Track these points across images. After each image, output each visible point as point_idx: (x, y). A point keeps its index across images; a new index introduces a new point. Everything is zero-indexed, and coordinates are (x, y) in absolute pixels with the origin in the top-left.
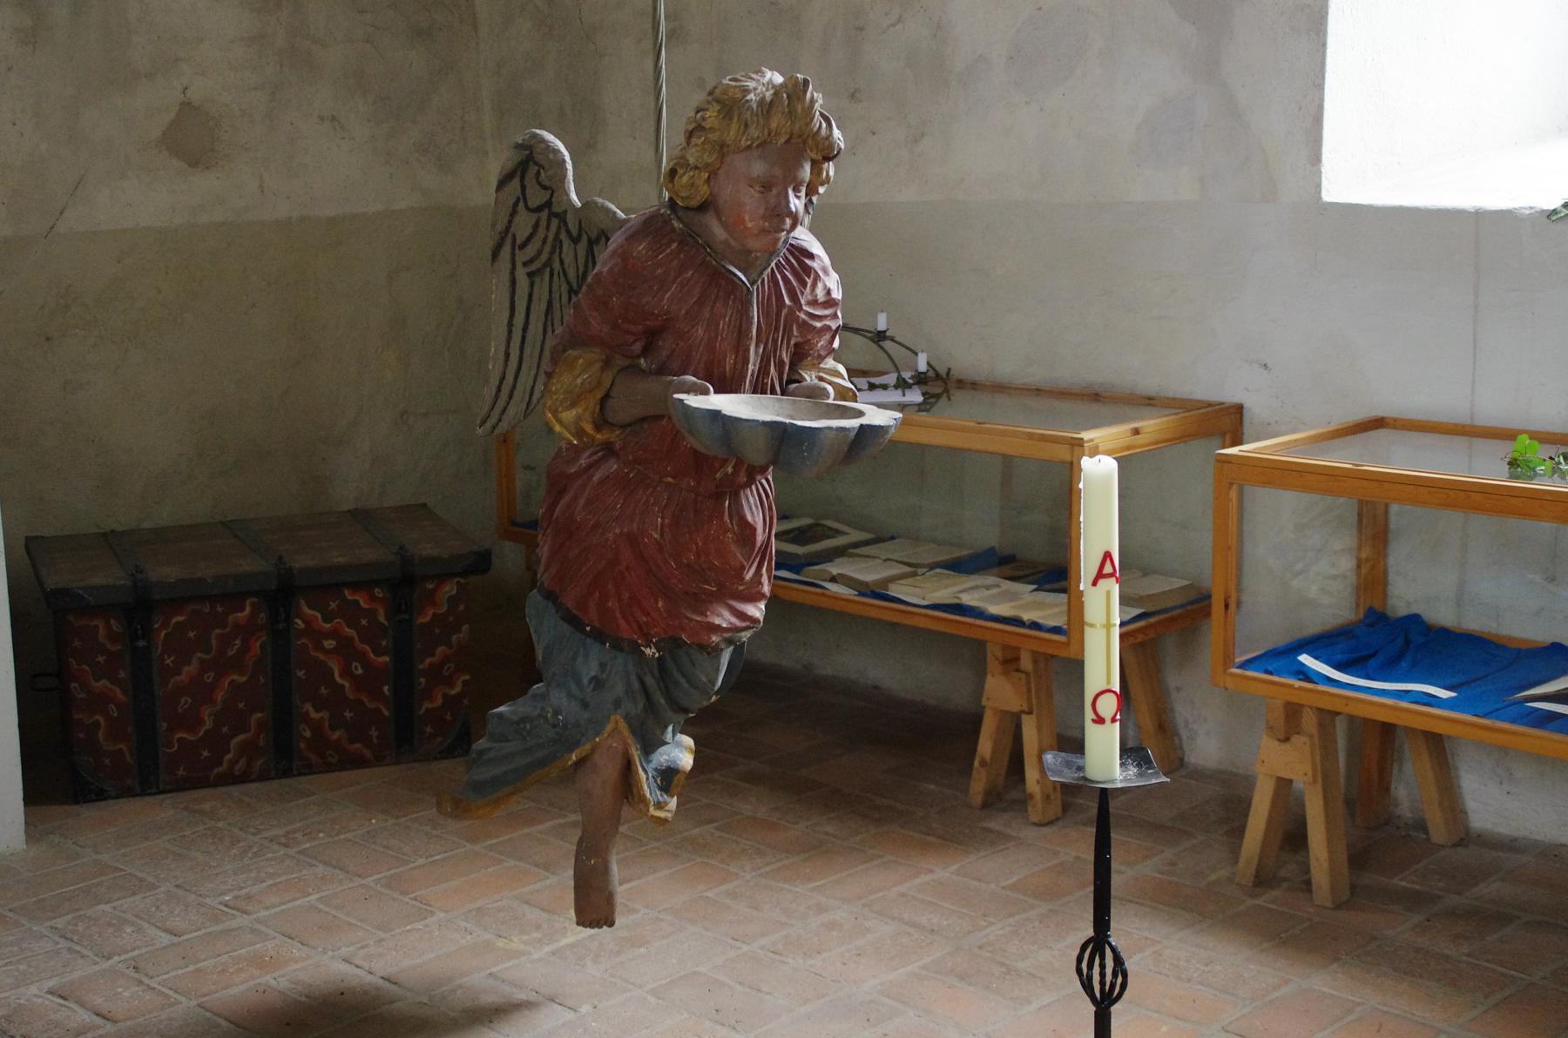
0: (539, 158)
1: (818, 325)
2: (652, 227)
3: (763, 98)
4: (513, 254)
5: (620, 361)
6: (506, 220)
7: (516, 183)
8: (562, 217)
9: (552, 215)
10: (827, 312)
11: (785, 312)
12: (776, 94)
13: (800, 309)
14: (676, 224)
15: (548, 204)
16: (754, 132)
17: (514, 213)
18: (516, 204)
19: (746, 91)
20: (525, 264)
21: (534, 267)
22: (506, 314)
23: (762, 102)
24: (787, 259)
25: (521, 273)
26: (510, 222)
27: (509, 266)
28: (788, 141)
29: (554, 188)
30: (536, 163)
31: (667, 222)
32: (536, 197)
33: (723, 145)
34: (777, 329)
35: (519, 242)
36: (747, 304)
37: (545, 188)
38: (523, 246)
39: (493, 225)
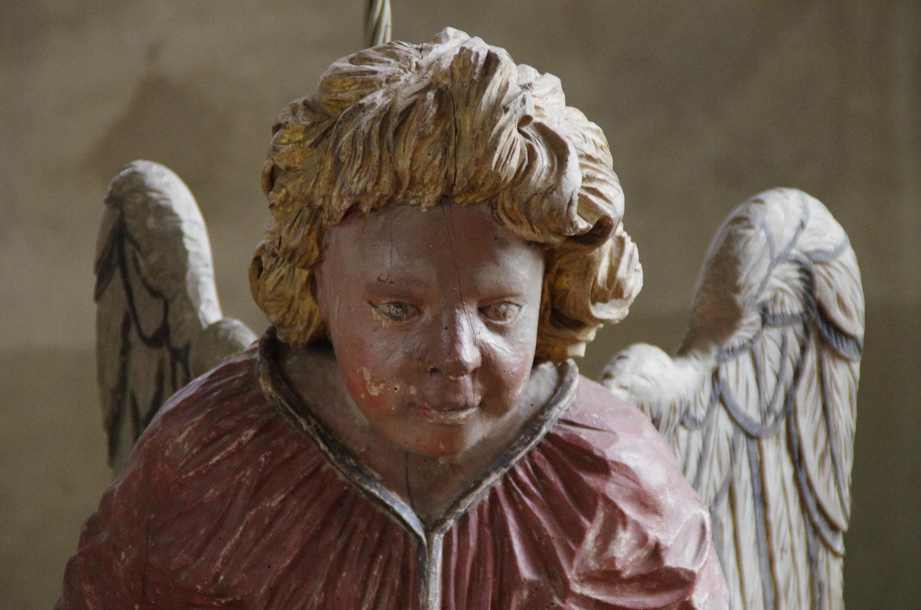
0: (132, 224)
6: (117, 364)
7: (117, 280)
13: (566, 592)
14: (266, 387)
16: (356, 182)
17: (126, 349)
19: (369, 84)
23: (387, 113)
24: (538, 474)
26: (124, 368)
28: (445, 199)
31: (250, 381)
37: (155, 294)
39: (101, 378)
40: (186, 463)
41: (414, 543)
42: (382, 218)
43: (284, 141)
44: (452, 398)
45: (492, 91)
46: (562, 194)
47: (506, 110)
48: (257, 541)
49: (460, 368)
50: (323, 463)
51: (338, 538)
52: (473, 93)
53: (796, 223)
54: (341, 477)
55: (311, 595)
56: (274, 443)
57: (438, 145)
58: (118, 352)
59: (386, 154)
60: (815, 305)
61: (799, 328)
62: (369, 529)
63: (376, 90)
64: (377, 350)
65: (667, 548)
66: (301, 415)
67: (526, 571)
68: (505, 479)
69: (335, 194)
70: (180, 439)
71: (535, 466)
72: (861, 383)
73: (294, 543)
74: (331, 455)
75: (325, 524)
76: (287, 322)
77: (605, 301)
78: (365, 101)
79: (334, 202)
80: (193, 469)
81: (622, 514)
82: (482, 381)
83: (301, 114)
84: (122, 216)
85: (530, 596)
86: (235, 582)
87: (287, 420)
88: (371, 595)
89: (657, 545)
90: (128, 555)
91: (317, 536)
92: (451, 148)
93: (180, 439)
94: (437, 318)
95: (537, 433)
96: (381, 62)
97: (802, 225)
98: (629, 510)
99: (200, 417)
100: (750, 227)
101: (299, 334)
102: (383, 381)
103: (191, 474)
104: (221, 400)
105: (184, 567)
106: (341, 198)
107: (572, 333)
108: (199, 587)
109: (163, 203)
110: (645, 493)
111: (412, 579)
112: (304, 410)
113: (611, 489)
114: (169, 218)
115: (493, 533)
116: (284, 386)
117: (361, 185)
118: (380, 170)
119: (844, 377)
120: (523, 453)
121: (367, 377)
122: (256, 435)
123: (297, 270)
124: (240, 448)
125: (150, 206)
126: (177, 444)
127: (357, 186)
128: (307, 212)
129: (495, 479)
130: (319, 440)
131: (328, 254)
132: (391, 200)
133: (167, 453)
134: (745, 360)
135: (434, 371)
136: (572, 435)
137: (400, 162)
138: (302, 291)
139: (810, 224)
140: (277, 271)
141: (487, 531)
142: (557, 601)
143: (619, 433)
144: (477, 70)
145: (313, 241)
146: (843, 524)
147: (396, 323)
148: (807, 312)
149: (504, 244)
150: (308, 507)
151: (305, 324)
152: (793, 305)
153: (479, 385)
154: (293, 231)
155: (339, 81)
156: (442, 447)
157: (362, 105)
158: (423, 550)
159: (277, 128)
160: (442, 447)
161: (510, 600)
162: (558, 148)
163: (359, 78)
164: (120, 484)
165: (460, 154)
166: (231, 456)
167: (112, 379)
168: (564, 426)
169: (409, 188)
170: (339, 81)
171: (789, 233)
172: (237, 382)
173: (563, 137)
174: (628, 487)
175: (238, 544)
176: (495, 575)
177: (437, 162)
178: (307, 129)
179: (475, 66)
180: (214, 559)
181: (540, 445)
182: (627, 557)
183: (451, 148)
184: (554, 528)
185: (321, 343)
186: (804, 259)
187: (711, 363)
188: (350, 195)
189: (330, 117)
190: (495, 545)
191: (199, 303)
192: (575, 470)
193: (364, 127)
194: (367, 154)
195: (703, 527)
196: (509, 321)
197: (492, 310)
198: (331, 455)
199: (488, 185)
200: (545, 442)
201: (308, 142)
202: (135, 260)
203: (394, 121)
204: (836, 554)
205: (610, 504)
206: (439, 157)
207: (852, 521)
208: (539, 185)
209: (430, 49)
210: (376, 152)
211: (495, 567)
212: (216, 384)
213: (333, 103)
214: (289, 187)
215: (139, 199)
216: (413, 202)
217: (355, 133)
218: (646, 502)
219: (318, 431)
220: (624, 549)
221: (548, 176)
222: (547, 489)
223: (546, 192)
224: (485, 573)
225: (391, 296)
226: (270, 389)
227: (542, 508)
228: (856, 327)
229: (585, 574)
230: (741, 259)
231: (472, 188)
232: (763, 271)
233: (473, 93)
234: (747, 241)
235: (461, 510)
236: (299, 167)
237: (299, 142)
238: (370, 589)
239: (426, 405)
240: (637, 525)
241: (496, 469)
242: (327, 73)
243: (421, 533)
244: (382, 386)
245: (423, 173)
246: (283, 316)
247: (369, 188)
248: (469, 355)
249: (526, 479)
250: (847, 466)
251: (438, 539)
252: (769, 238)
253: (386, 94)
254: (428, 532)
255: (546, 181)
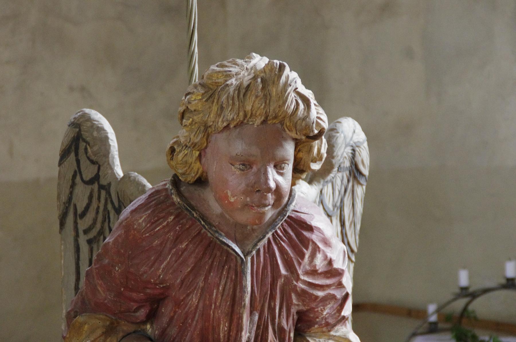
0: (85, 135)
1: (320, 294)
2: (158, 202)
3: (241, 84)
4: (76, 223)
5: (126, 327)
6: (68, 192)
8: (106, 188)
9: (101, 187)
10: (328, 282)
11: (280, 282)
12: (255, 78)
13: (298, 279)
14: (176, 199)
15: (96, 178)
16: (229, 115)
17: (73, 185)
18: (74, 177)
19: (229, 76)
20: (86, 232)
21: (91, 235)
22: (73, 278)
23: (239, 88)
24: (285, 232)
25: (83, 240)
26: (71, 193)
27: (73, 233)
28: (264, 122)
29: (101, 161)
30: (84, 141)
31: (168, 197)
32: (89, 172)
33: (206, 127)
34: (273, 297)
35: (79, 211)
36: (239, 275)
37: (93, 162)
38: (83, 215)
39: (59, 197)
40: (145, 231)
41: (239, 261)
42: (238, 130)
43: (193, 99)
44: (263, 202)
45: (283, 79)
46: (310, 119)
47: (290, 85)
48: (176, 262)
49: (269, 190)
50: (202, 229)
51: (209, 259)
52: (276, 79)
53: (353, 131)
54: (209, 235)
55: (198, 282)
56: (181, 222)
57: (263, 100)
58: (69, 187)
59: (241, 104)
60: (354, 163)
61: (348, 172)
62: (221, 255)
63: (232, 78)
64: (233, 182)
65: (334, 260)
66: (193, 210)
67: (283, 271)
68: (273, 235)
69: (220, 120)
70: (140, 221)
71: (284, 229)
72: (365, 194)
73: (191, 261)
74: (206, 226)
75: (204, 254)
76: (187, 173)
77: (315, 162)
78: (229, 82)
79: (219, 123)
80: (148, 233)
81: (319, 248)
82: (275, 195)
83: (199, 88)
84: (80, 130)
85: (284, 281)
86: (167, 278)
87: (186, 212)
88: (223, 282)
89: (331, 260)
90: (119, 268)
91: (201, 259)
92: (268, 101)
93: (140, 221)
94: (259, 170)
95: (285, 216)
96: (231, 67)
97: (354, 132)
98: (321, 245)
99: (149, 212)
100: (338, 132)
101: (192, 177)
102: (236, 196)
103: (147, 235)
104: (157, 205)
105: (145, 272)
106: (223, 122)
107: (299, 175)
108: (152, 280)
109: (100, 125)
110: (326, 238)
111: (239, 275)
112: (193, 209)
113: (314, 237)
114: (102, 132)
115: (269, 256)
116: (184, 199)
117: (231, 116)
118: (239, 110)
119: (360, 191)
120: (280, 225)
121: (229, 194)
122: (174, 219)
123: (194, 151)
124: (168, 224)
125: (94, 127)
126: (140, 223)
127: (230, 117)
128: (202, 128)
129: (270, 235)
130: (201, 220)
131: (210, 145)
132: (242, 122)
133: (135, 226)
134: (330, 185)
135: (258, 191)
136: (297, 216)
137: (247, 107)
138: (196, 160)
139: (356, 131)
140: (183, 152)
141: (267, 255)
142: (295, 283)
143: (315, 215)
144: (277, 70)
145: (205, 140)
146: (355, 250)
147: (242, 172)
148: (351, 166)
149: (285, 140)
150: (197, 247)
151: (196, 173)
152: (347, 164)
153: (273, 196)
154: (196, 135)
155: (216, 75)
156: (257, 222)
157: (227, 85)
158: (243, 263)
159: (189, 94)
160: (257, 222)
161: (277, 283)
162: (306, 101)
163: (225, 74)
164: (113, 239)
165: (271, 103)
166: (164, 227)
167: (64, 198)
168: (294, 212)
169: (250, 118)
170: (216, 75)
171: (350, 135)
172: (162, 198)
173: (307, 96)
174: (320, 236)
175: (168, 263)
176: (271, 273)
177: (262, 107)
178: (203, 94)
179: (276, 68)
180: (158, 269)
181: (285, 220)
182: (320, 264)
183: (268, 101)
184: (293, 253)
185: (201, 181)
186: (354, 145)
187: (321, 187)
188: (227, 121)
189: (212, 89)
190: (270, 261)
191: (114, 166)
192: (300, 230)
193: (232, 93)
194: (233, 104)
195: (344, 252)
196: (285, 170)
197: (279, 167)
198: (206, 226)
199: (282, 116)
200: (287, 219)
201: (204, 100)
202: (86, 149)
203: (243, 91)
204: (352, 261)
205: (313, 242)
206: (264, 105)
207: (358, 249)
208: (301, 116)
209: (250, 62)
210: (237, 103)
211: (271, 269)
212: (153, 199)
213: (214, 84)
214: (195, 118)
215: (89, 124)
216: (251, 123)
217: (228, 96)
218: (326, 242)
219: (200, 216)
220: (319, 263)
221: (304, 112)
222: (290, 238)
223: (304, 119)
224: (267, 272)
225: (240, 161)
226: (179, 200)
227: (288, 245)
228: (366, 171)
229: (305, 272)
230: (335, 145)
231: (276, 117)
232: (342, 150)
233: (276, 79)
234: (337, 138)
235: (258, 247)
236: (200, 110)
237: (200, 99)
238: (222, 279)
239: (254, 205)
240: (323, 251)
241: (271, 230)
242: (209, 72)
243: (243, 257)
244: (235, 198)
245: (256, 111)
246: (186, 170)
247: (235, 117)
248: (273, 185)
249: (281, 234)
250: (358, 227)
251: (249, 259)
252: (345, 137)
253: (236, 80)
254: (246, 256)
255: (303, 114)
